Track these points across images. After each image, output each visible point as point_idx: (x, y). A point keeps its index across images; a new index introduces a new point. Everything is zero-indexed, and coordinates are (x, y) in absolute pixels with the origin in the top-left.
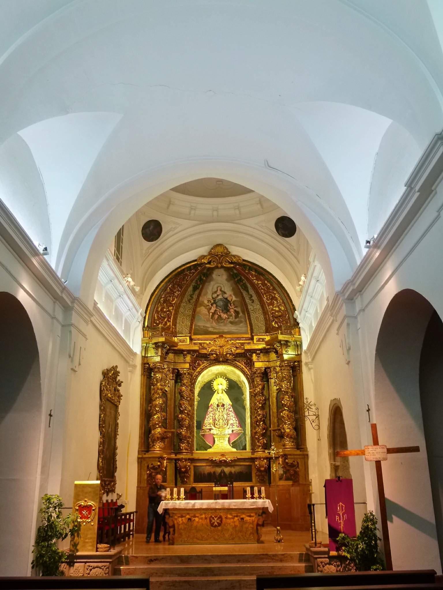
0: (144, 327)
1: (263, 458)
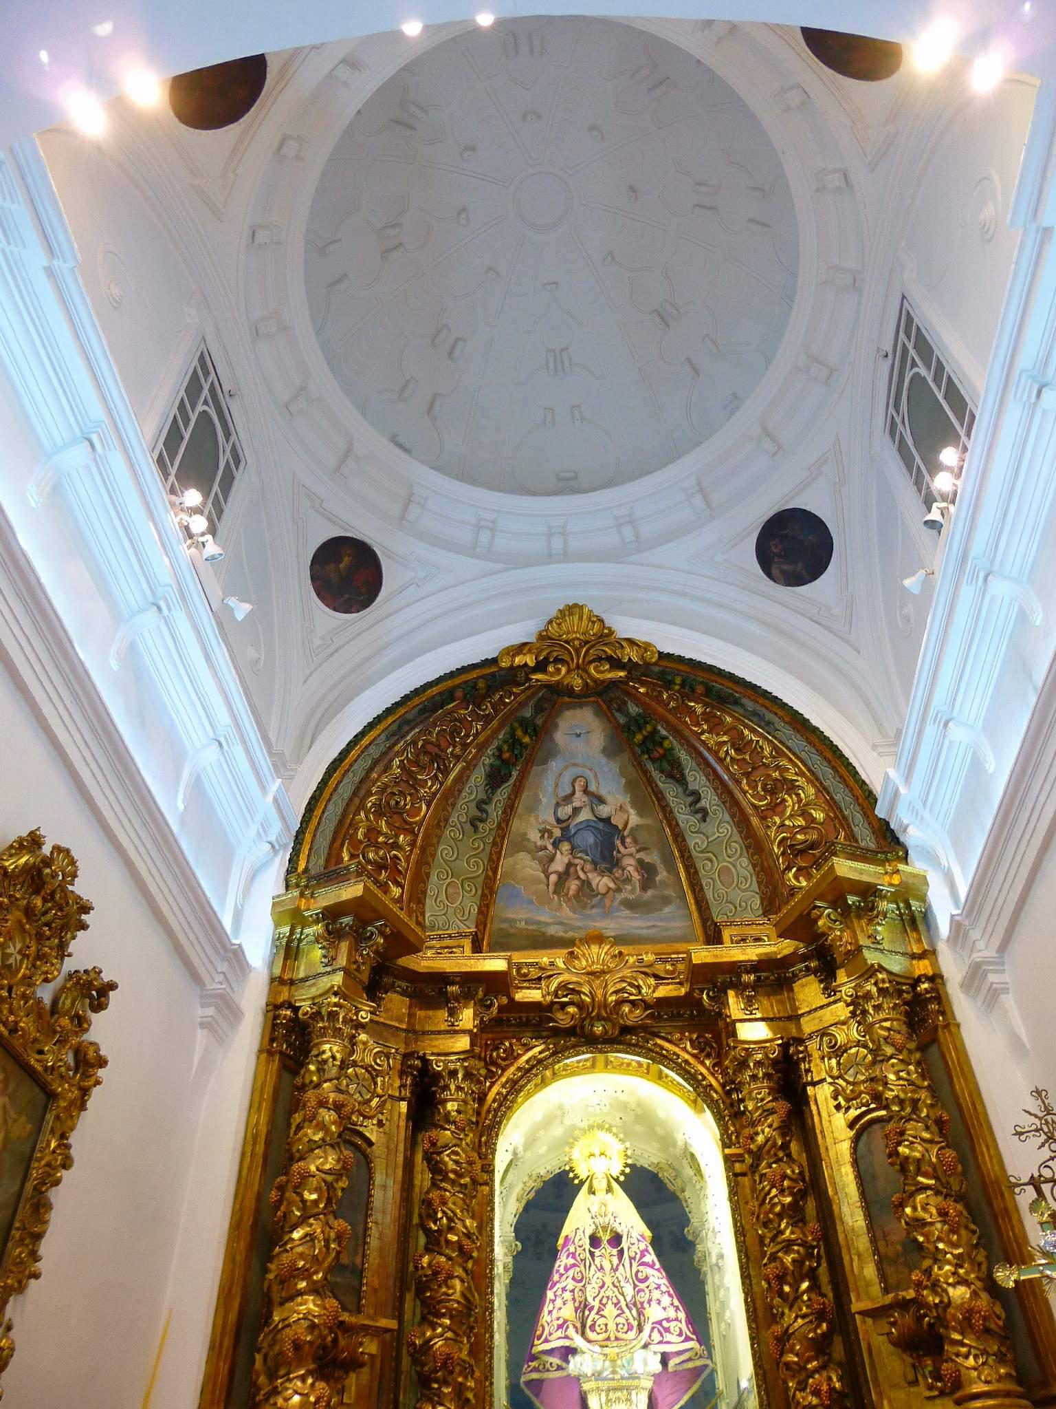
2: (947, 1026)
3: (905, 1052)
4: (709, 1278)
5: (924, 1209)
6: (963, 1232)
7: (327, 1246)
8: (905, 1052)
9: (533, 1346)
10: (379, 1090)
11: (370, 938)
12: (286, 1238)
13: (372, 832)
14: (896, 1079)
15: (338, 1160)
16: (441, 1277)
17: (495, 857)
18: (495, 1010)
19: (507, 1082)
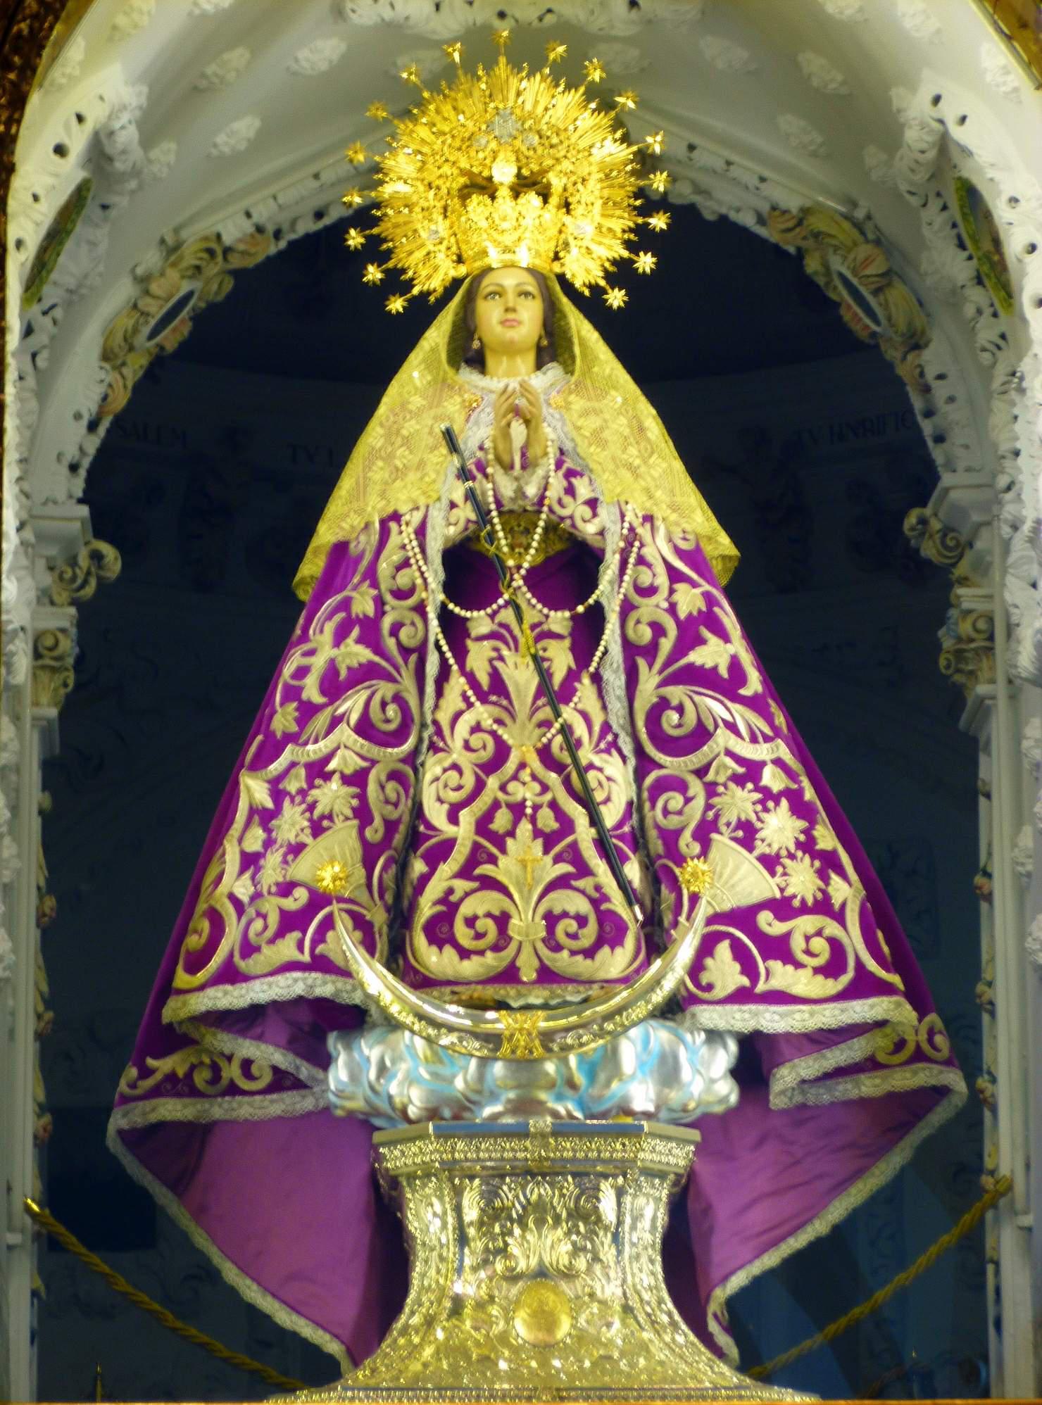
4: (998, 729)
9: (167, 990)
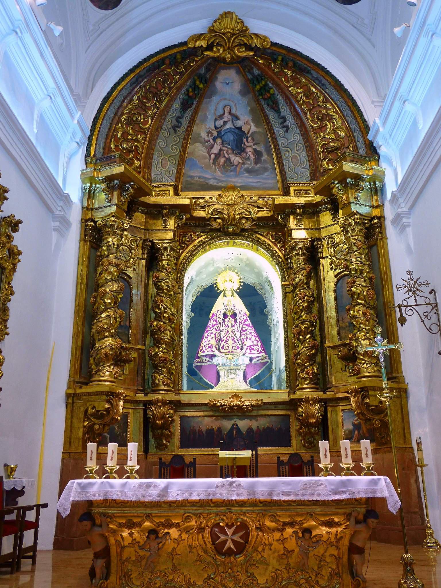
0: (87, 155)
1: (313, 400)
2: (382, 239)
3: (362, 250)
5: (358, 312)
6: (371, 321)
7: (116, 320)
8: (362, 250)
10: (133, 256)
11: (127, 190)
12: (99, 317)
13: (125, 134)
14: (356, 260)
15: (118, 287)
16: (162, 330)
17: (184, 145)
18: (184, 220)
19: (189, 251)
